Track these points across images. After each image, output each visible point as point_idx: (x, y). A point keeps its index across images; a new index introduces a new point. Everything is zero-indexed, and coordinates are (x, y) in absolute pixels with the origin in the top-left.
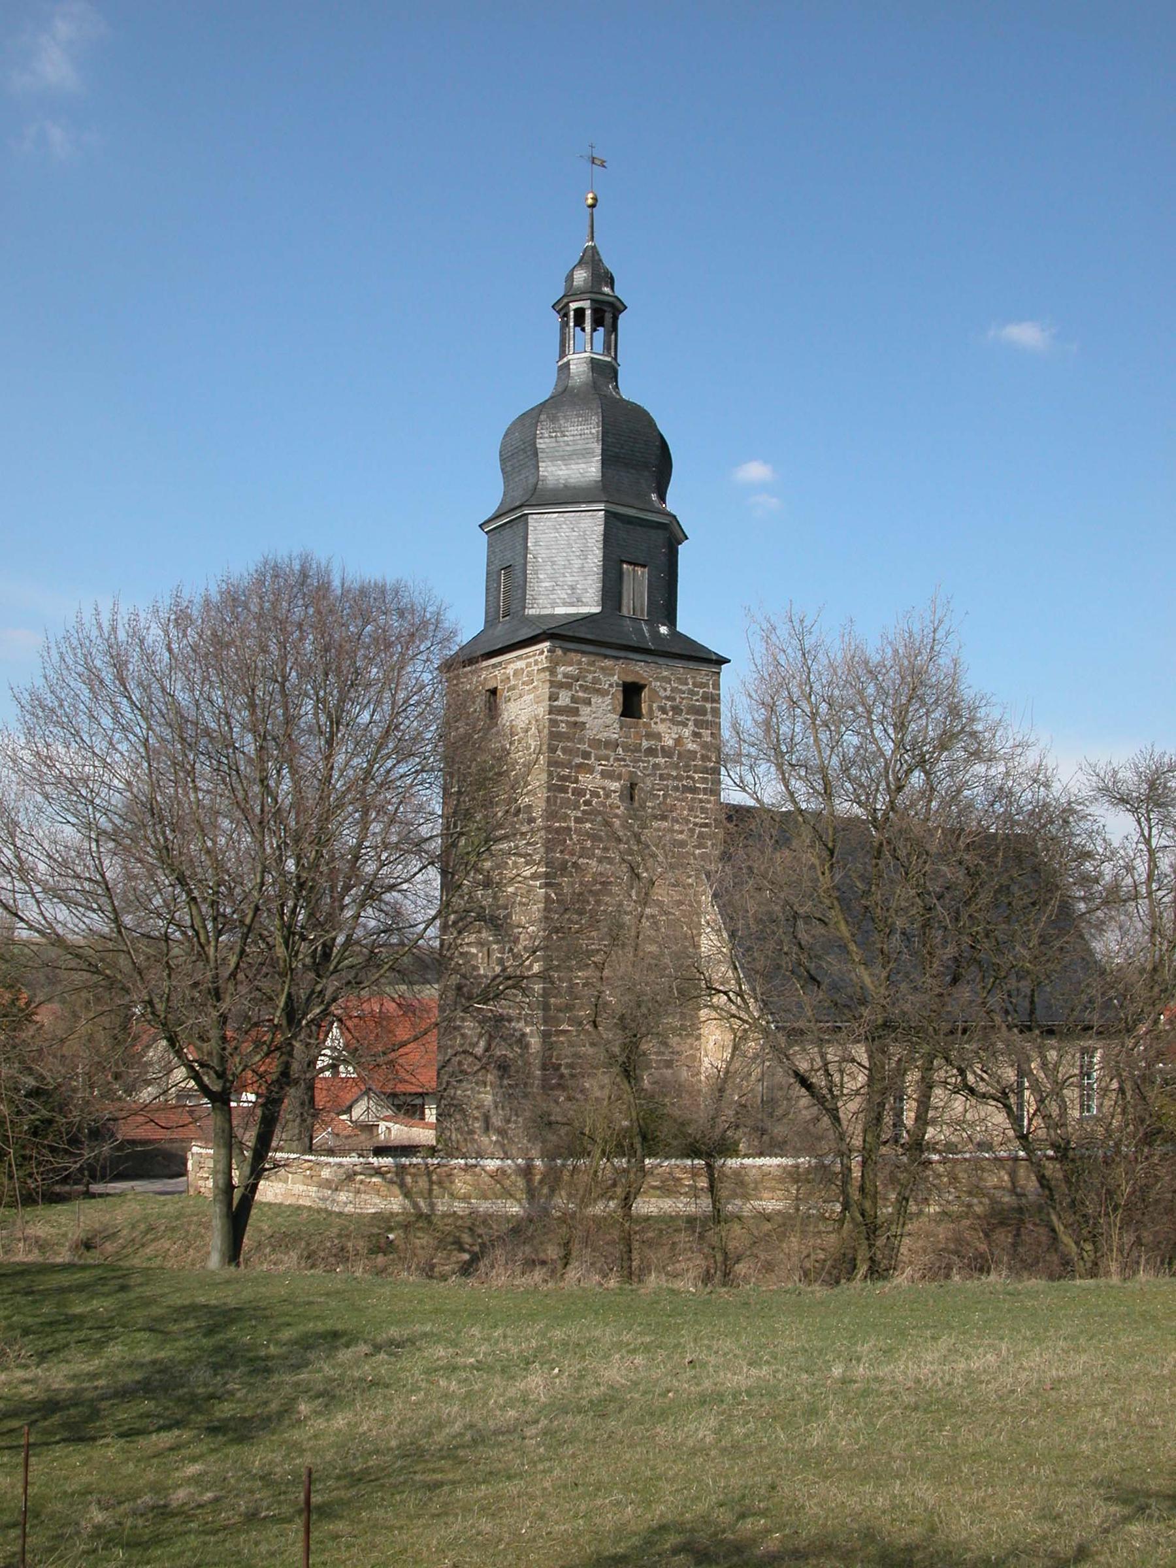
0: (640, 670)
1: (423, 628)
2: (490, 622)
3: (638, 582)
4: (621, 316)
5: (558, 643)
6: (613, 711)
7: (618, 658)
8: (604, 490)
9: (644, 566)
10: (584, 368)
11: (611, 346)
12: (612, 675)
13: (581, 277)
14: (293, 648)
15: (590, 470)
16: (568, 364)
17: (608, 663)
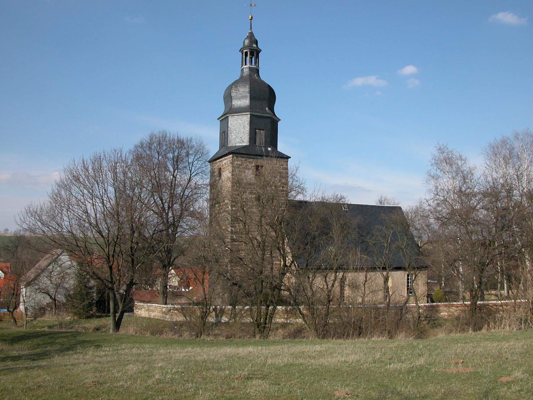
0: (260, 162)
1: (200, 151)
2: (221, 148)
3: (261, 135)
4: (260, 54)
5: (234, 155)
6: (253, 174)
7: (254, 158)
8: (251, 109)
9: (263, 130)
10: (248, 70)
11: (257, 62)
12: (252, 163)
13: (247, 42)
14: (160, 159)
15: (245, 102)
16: (243, 69)
17: (251, 160)
